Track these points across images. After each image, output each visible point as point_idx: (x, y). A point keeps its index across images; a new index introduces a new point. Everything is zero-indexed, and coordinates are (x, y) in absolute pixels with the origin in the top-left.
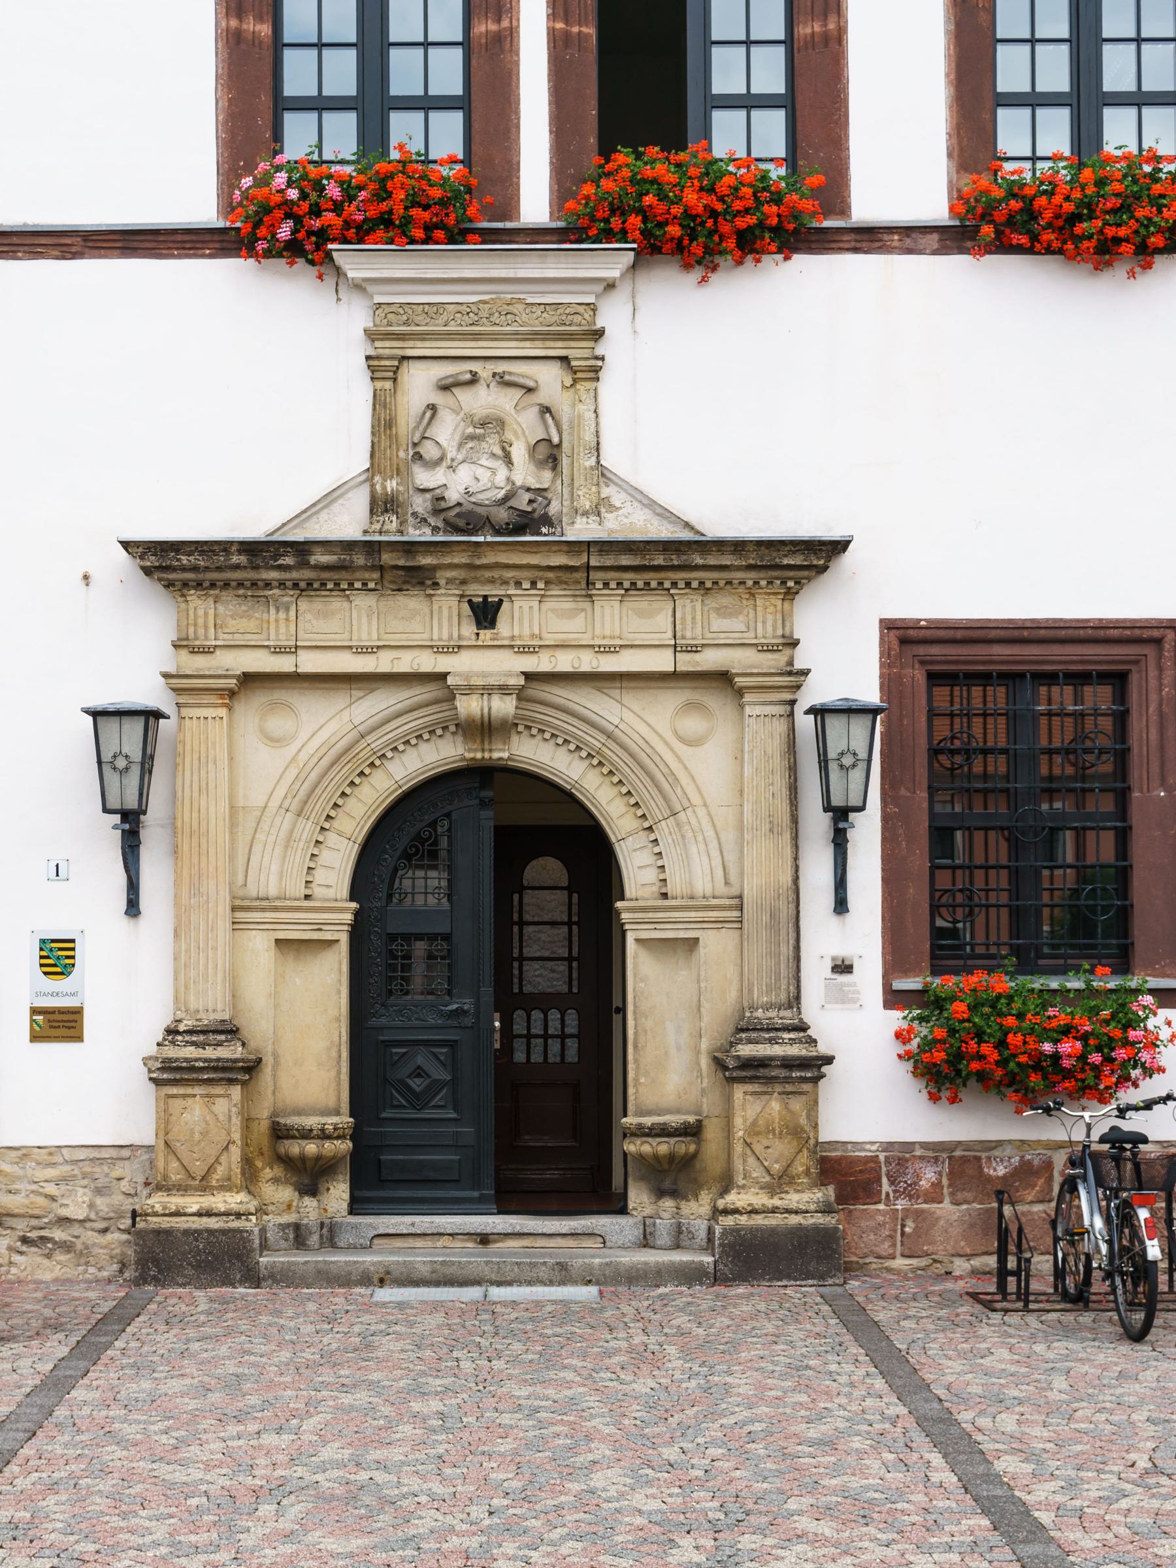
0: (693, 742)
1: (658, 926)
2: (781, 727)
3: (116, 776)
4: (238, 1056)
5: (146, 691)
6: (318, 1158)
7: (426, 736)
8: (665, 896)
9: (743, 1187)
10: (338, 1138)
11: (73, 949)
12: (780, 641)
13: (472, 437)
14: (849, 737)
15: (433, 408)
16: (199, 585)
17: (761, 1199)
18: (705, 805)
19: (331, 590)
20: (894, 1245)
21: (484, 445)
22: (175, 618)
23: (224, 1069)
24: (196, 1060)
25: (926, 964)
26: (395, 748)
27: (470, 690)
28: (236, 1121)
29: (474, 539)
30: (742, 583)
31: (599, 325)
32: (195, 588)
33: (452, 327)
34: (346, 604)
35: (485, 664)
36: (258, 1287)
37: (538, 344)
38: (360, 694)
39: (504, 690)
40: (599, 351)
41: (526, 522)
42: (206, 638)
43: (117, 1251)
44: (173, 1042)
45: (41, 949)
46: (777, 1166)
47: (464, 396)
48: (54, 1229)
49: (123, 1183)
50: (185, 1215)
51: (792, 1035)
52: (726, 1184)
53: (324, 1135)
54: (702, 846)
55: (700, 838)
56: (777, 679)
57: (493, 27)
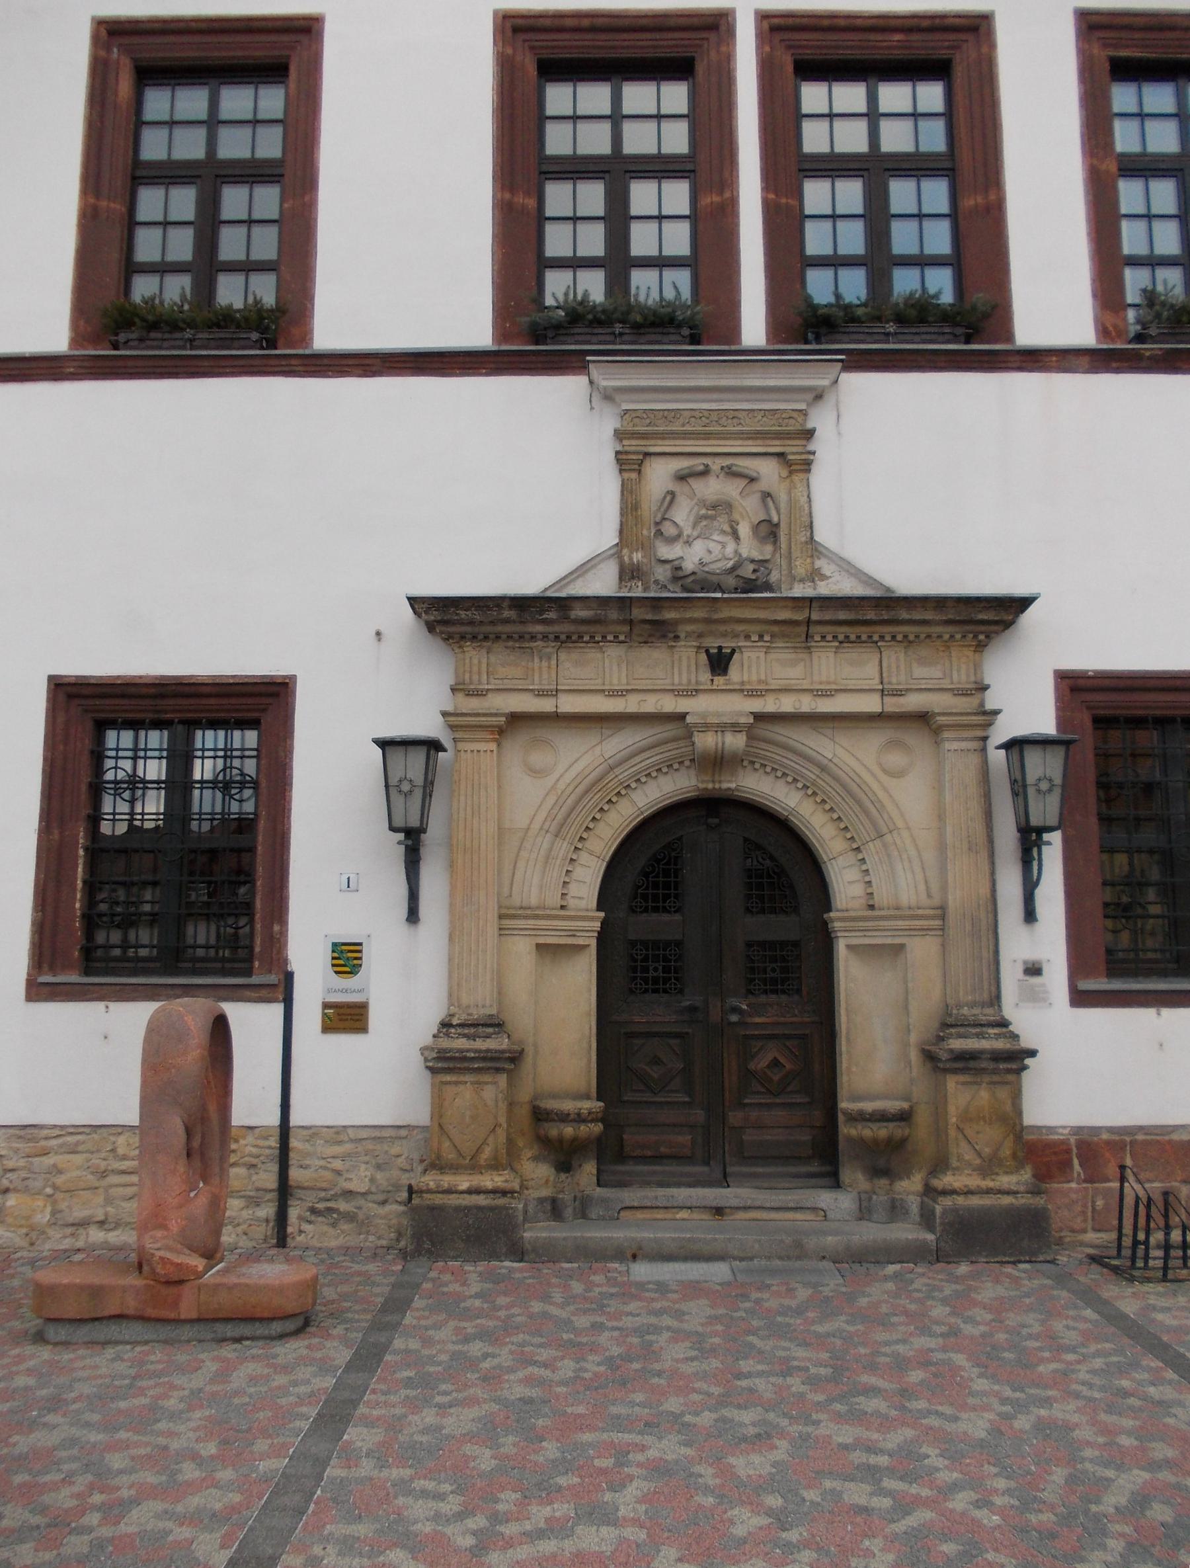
0: (899, 774)
1: (870, 934)
2: (974, 760)
3: (401, 799)
4: (504, 1047)
5: (427, 725)
6: (574, 1139)
7: (665, 770)
8: (872, 907)
9: (957, 1169)
10: (592, 1121)
11: (360, 951)
12: (973, 686)
13: (705, 517)
14: (1039, 766)
15: (672, 494)
16: (474, 638)
17: (974, 1182)
18: (908, 828)
19: (587, 642)
20: (1085, 1221)
21: (715, 523)
22: (452, 670)
23: (492, 1059)
24: (468, 1051)
25: (1102, 967)
26: (638, 780)
27: (706, 727)
28: (503, 1106)
29: (713, 595)
30: (940, 637)
31: (810, 425)
32: (470, 640)
33: (688, 428)
34: (599, 655)
35: (719, 705)
36: (521, 1261)
37: (759, 442)
38: (608, 732)
39: (735, 727)
40: (811, 447)
41: (750, 586)
42: (480, 683)
43: (394, 1221)
44: (447, 1035)
45: (333, 951)
46: (987, 1150)
47: (697, 485)
48: (340, 1200)
49: (400, 1160)
50: (456, 1192)
51: (996, 1030)
52: (940, 1165)
53: (580, 1119)
54: (906, 864)
55: (905, 856)
56: (974, 718)
57: (716, 199)
